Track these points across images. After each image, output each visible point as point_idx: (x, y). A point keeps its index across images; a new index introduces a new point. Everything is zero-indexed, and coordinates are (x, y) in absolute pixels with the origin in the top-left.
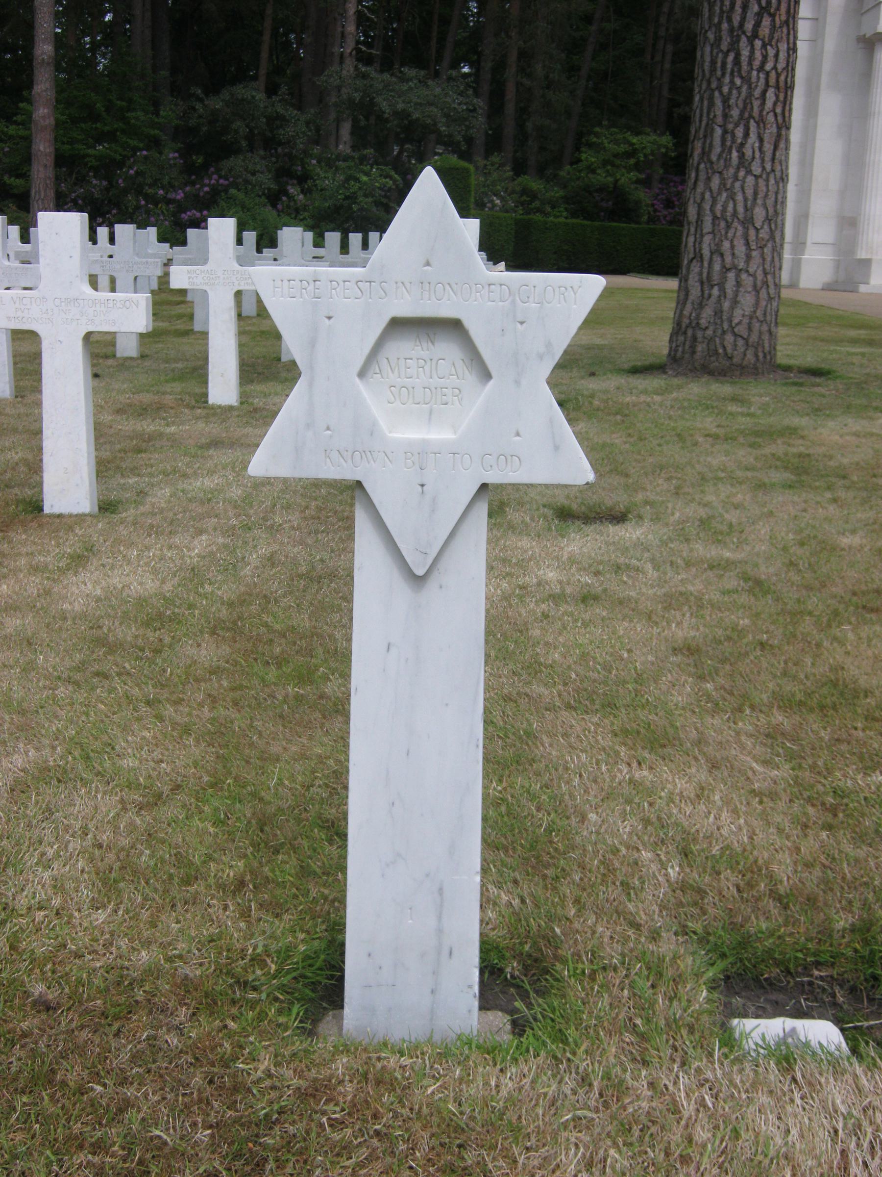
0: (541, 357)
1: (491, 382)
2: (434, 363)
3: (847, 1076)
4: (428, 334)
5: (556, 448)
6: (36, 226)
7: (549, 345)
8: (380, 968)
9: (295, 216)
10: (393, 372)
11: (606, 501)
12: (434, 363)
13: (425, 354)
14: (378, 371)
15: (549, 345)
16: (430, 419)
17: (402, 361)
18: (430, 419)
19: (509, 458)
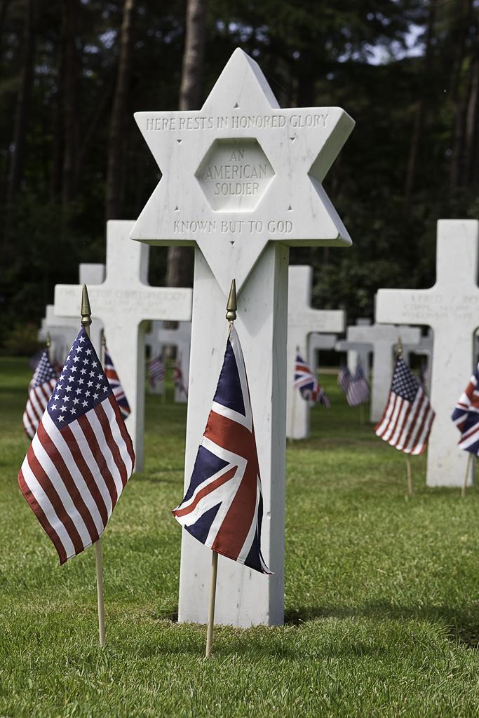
0: (304, 159)
1: (275, 176)
2: (243, 167)
3: (363, 383)
4: (239, 151)
5: (314, 216)
6: (52, 302)
7: (309, 151)
8: (203, 586)
9: (441, 608)
10: (218, 175)
11: (404, 341)
12: (243, 167)
13: (238, 163)
14: (209, 174)
15: (309, 151)
16: (240, 202)
17: (224, 168)
18: (240, 202)
19: (285, 223)
